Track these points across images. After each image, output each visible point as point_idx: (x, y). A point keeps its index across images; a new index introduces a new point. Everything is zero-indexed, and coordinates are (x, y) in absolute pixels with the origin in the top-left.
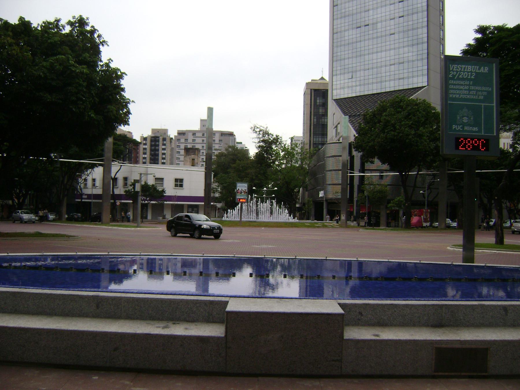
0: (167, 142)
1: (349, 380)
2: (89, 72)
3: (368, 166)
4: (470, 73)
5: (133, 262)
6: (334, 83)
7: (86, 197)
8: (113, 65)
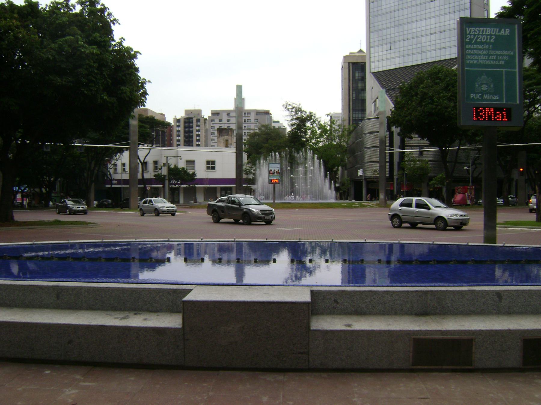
0: (201, 123)
1: (317, 374)
2: (99, 52)
3: (407, 141)
4: (489, 37)
5: (170, 248)
6: (372, 55)
7: (116, 182)
8: (125, 44)
